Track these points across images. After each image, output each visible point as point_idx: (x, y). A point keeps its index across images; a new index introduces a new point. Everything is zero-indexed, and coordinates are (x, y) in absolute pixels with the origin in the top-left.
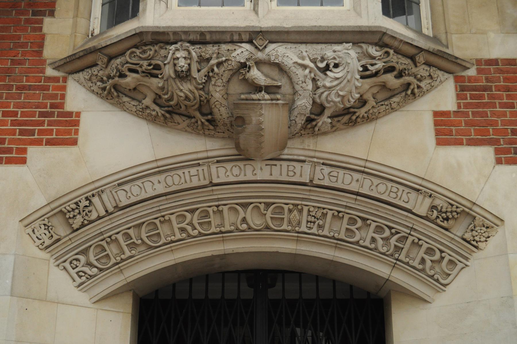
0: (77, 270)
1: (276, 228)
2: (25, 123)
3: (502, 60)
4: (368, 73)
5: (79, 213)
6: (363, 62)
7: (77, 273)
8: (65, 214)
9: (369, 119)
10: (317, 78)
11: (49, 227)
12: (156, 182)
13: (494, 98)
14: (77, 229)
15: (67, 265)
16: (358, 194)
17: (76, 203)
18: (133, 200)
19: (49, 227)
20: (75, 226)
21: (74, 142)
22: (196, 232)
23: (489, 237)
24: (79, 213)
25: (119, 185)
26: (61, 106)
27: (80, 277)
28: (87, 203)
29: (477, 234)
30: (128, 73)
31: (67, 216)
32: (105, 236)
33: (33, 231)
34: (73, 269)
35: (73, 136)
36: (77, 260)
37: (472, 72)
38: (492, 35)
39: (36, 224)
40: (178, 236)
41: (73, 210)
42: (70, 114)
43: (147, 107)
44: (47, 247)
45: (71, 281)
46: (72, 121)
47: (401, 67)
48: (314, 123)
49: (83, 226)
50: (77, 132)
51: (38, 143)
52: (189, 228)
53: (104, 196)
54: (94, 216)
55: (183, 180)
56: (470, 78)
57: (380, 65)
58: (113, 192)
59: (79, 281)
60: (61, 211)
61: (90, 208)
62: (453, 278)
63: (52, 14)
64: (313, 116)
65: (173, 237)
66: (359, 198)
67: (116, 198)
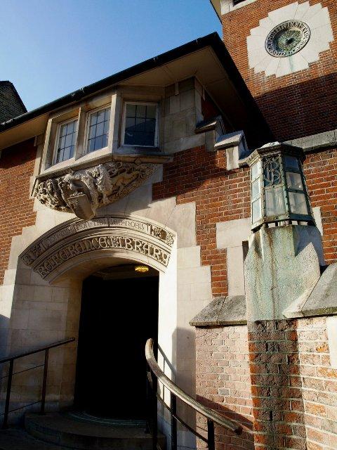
42: (34, 213)
46: (34, 216)
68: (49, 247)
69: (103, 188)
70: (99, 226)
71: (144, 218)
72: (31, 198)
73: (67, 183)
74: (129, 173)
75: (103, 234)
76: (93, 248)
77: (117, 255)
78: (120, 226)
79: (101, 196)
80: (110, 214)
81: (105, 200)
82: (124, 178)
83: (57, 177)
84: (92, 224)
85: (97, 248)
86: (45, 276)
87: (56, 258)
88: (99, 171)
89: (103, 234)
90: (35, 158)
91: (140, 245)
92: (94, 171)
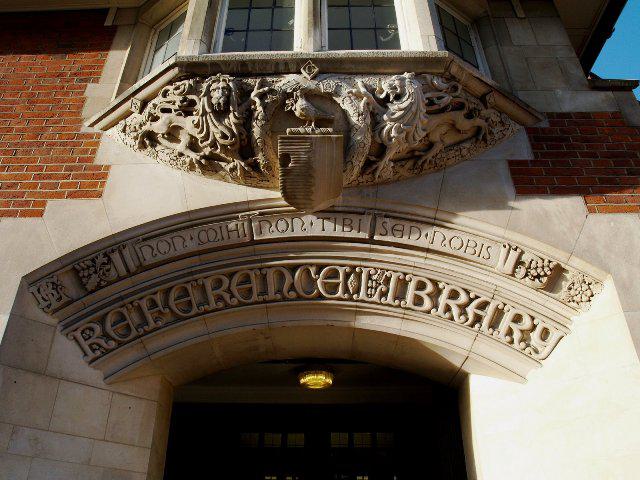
0: (90, 341)
1: (330, 296)
2: (49, 177)
3: (574, 114)
4: (435, 107)
5: (96, 272)
6: (429, 95)
7: (90, 346)
8: (79, 272)
9: (438, 167)
10: (376, 111)
11: (57, 286)
12: (188, 238)
13: (574, 148)
14: (92, 292)
15: (78, 334)
16: (428, 250)
17: (93, 260)
18: (160, 258)
19: (57, 286)
20: (89, 287)
21: (99, 195)
22: (235, 301)
23: (592, 296)
24: (96, 272)
25: (144, 240)
26: (90, 160)
27: (94, 350)
28: (105, 260)
29: (579, 296)
30: (160, 114)
31: (81, 275)
32: (126, 301)
33: (39, 291)
34: (86, 340)
35: (98, 189)
36: (92, 329)
37: (545, 124)
38: (560, 92)
39: (43, 283)
40: (213, 305)
41: (88, 267)
42: (99, 168)
43: (181, 155)
44: (56, 311)
45: (81, 354)
46: (100, 175)
47: (472, 106)
48: (375, 166)
49: (99, 287)
50: (103, 184)
51: (60, 196)
52: (227, 296)
53: (126, 252)
54: (113, 274)
55: (219, 237)
56: (543, 130)
57: (447, 99)
58: (136, 248)
59: (91, 355)
60: (74, 268)
61: (108, 267)
62: (549, 350)
63: (96, 81)
64: (373, 159)
65: (206, 306)
66: (429, 255)
67: (140, 255)
68: (142, 268)
69: (399, 131)
70: (338, 233)
71: (500, 231)
72: (85, 128)
73: (289, 96)
74: (469, 116)
75: (339, 259)
76: (293, 294)
77: (366, 322)
78: (411, 242)
79: (381, 149)
80: (382, 206)
81: (385, 167)
82: (453, 126)
83: (249, 75)
84: (311, 225)
85: (308, 296)
86: (97, 354)
87: (154, 304)
88: (403, 86)
89: (339, 259)
90: (108, 49)
91: (463, 298)
92: (385, 85)
